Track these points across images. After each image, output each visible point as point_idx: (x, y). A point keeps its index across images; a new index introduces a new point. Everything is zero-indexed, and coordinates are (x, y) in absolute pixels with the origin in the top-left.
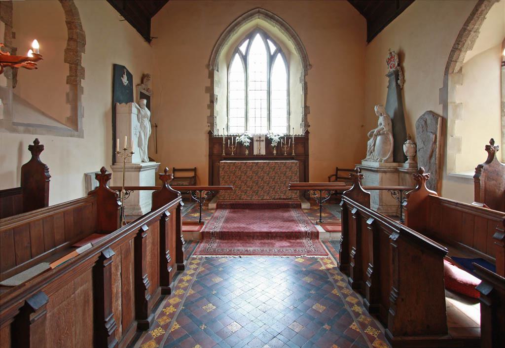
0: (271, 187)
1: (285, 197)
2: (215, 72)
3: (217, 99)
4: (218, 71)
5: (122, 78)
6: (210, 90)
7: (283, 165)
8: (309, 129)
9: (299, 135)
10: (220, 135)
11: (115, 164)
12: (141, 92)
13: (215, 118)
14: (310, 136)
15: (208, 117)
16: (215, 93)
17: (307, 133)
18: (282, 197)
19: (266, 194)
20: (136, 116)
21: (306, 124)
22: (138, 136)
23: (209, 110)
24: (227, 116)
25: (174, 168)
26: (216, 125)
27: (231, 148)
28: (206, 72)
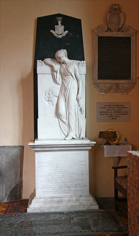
5: (52, 31)
20: (51, 76)
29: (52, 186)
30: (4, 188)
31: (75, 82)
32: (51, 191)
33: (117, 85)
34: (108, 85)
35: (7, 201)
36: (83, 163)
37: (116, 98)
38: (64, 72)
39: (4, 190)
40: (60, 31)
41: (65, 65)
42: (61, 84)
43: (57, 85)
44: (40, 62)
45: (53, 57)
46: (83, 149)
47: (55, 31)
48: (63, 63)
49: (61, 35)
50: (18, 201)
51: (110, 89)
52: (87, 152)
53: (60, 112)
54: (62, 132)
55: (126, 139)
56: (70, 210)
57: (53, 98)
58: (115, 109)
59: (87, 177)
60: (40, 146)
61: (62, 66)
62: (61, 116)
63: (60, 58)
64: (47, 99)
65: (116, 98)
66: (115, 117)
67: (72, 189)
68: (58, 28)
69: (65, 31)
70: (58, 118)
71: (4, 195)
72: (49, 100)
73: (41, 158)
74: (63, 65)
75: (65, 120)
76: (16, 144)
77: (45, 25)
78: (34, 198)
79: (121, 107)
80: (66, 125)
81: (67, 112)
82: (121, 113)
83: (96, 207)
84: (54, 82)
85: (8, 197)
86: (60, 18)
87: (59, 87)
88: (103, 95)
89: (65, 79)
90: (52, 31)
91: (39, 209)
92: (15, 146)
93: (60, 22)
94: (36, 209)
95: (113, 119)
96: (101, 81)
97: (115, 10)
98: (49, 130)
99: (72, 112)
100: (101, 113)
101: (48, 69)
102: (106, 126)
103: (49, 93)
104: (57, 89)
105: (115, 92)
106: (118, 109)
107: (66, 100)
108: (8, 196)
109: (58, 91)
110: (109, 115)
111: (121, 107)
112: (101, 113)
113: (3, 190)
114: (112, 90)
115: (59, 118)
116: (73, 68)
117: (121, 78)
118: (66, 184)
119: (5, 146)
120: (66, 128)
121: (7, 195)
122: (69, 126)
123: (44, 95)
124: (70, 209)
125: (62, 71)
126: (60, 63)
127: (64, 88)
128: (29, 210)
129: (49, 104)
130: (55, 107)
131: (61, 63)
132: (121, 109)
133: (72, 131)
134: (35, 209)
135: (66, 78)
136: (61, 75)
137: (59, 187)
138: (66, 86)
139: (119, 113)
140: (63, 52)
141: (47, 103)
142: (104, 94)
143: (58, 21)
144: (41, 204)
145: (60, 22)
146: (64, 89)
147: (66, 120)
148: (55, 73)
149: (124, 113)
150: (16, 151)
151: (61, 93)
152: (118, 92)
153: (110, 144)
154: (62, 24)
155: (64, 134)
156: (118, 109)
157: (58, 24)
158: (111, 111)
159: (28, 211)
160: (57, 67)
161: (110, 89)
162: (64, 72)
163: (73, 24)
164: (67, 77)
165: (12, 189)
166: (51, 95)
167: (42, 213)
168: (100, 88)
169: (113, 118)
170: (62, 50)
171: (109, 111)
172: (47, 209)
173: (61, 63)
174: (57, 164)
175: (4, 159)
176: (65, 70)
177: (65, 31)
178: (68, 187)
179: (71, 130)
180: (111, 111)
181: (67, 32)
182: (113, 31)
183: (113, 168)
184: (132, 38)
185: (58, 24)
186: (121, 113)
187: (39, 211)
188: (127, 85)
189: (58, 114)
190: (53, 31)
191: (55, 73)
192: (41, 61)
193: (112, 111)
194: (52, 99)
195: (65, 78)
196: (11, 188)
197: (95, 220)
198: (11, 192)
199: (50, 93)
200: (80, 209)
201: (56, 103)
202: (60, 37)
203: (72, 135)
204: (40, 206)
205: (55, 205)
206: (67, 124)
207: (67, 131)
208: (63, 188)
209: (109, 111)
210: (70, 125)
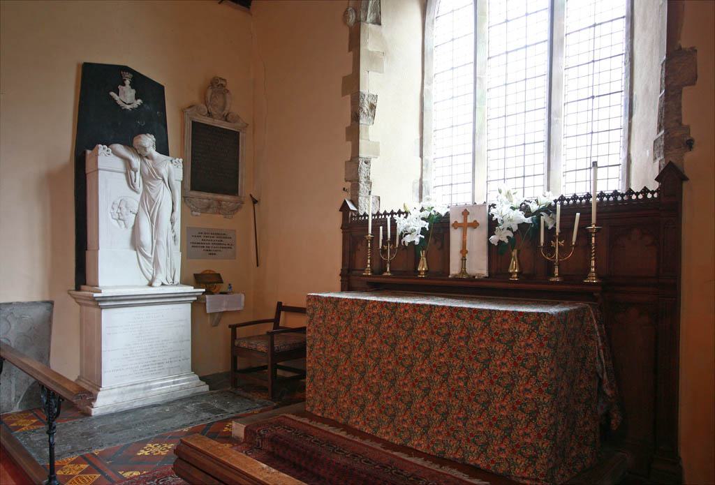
0: (433, 406)
1: (481, 463)
2: (368, 29)
3: (373, 107)
4: (378, 22)
5: (112, 94)
6: (352, 84)
7: (478, 324)
8: (689, 160)
9: (575, 197)
10: (382, 212)
11: (83, 287)
12: (194, 123)
13: (362, 165)
14: (690, 195)
15: (346, 162)
16: (361, 90)
17: (671, 176)
18: (471, 460)
19: (418, 430)
20: (123, 176)
21: (675, 135)
22: (131, 224)
23: (349, 143)
24: (421, 156)
25: (279, 304)
26: (369, 183)
27: (384, 252)
28: (345, 34)
29: (131, 365)
30: (13, 385)
31: (167, 193)
32: (130, 375)
33: (219, 202)
34: (205, 201)
35: (20, 410)
36: (182, 323)
37: (215, 222)
38: (149, 173)
39: (13, 390)
40: (127, 97)
41: (151, 161)
42: (141, 193)
43: (135, 193)
44: (104, 149)
45: (129, 144)
46: (110, 301)
47: (118, 95)
48: (147, 157)
49: (129, 104)
50: (59, 402)
51: (209, 207)
52: (189, 306)
53: (142, 240)
54: (143, 275)
55: (230, 285)
56: (167, 399)
57: (127, 215)
58: (215, 239)
59: (188, 345)
60: (114, 298)
61: (145, 162)
62: (143, 247)
63: (145, 148)
64: (117, 217)
65: (215, 222)
66: (214, 252)
67: (166, 366)
68: (124, 92)
69: (136, 99)
70: (136, 250)
71: (13, 399)
72: (119, 219)
73: (111, 320)
74: (147, 160)
75: (149, 255)
76: (36, 297)
77: (97, 81)
78: (99, 391)
79: (223, 236)
80: (150, 262)
81: (155, 241)
82: (224, 246)
83: (205, 388)
84: (131, 187)
85: (22, 401)
86: (130, 75)
87: (138, 197)
88: (197, 215)
89: (149, 185)
90: (112, 94)
91: (114, 407)
92: (35, 302)
93: (128, 82)
94: (109, 408)
95: (210, 254)
96: (195, 193)
97: (217, 86)
98: (115, 269)
99: (163, 240)
100: (194, 245)
101: (119, 164)
102: (202, 266)
103: (120, 206)
104: (134, 199)
105: (215, 213)
106: (218, 239)
107: (152, 221)
108: (21, 399)
109: (136, 204)
110: (205, 248)
111: (223, 236)
112: (194, 245)
113: (10, 390)
114: (211, 210)
115: (138, 251)
116: (167, 167)
117: (226, 193)
118: (156, 359)
119: (11, 304)
120: (150, 266)
121: (19, 397)
122: (156, 263)
123: (109, 209)
124: (167, 396)
125: (146, 170)
126: (140, 156)
127: (150, 202)
128: (95, 412)
129: (121, 226)
130: (130, 231)
131: (142, 155)
132: (223, 240)
133: (161, 273)
134: (107, 406)
135: (153, 183)
136: (142, 177)
137: (144, 366)
138: (153, 197)
139: (219, 246)
140: (150, 139)
141: (115, 222)
142: (199, 214)
143: (125, 80)
144: (115, 398)
145: (128, 82)
146: (148, 201)
147: (152, 254)
148: (133, 173)
149: (227, 246)
150: (40, 311)
151: (143, 207)
152: (220, 214)
153: (212, 294)
154: (133, 86)
155: (146, 277)
156: (218, 239)
157: (124, 85)
158: (208, 242)
159: (93, 414)
160: (136, 162)
161: (209, 207)
162: (149, 173)
163: (149, 90)
164: (154, 181)
165: (30, 384)
166: (124, 210)
167: (120, 412)
168: (193, 205)
169: (211, 252)
170: (149, 135)
171: (206, 242)
172: (128, 404)
173: (142, 155)
174: (141, 327)
175: (13, 328)
176: (151, 169)
177: (136, 99)
178: (159, 364)
179: (159, 271)
180: (208, 242)
181: (139, 101)
182: (215, 116)
183: (230, 326)
184: (240, 134)
185: (124, 85)
186: (224, 246)
187: (113, 411)
188: (232, 204)
189: (136, 243)
190: (117, 96)
191: (133, 173)
192: (105, 146)
193: (210, 242)
194: (126, 217)
195: (150, 183)
196: (29, 383)
197: (218, 401)
198: (28, 391)
199: (123, 206)
200: (182, 395)
201: (133, 224)
202: (128, 107)
203: (161, 278)
204: (115, 401)
205: (141, 395)
206: (152, 261)
207: (151, 271)
208: (150, 367)
209: (206, 242)
210: (159, 263)
